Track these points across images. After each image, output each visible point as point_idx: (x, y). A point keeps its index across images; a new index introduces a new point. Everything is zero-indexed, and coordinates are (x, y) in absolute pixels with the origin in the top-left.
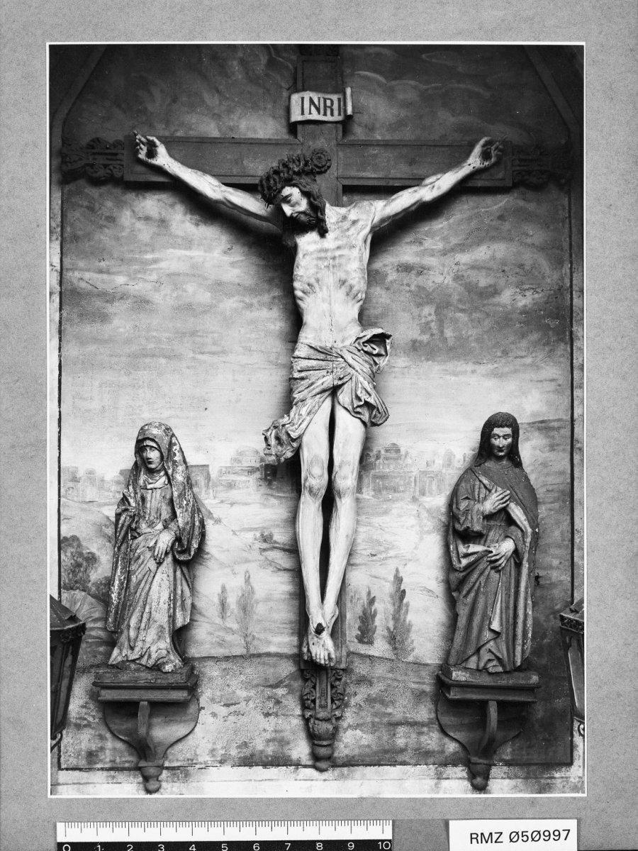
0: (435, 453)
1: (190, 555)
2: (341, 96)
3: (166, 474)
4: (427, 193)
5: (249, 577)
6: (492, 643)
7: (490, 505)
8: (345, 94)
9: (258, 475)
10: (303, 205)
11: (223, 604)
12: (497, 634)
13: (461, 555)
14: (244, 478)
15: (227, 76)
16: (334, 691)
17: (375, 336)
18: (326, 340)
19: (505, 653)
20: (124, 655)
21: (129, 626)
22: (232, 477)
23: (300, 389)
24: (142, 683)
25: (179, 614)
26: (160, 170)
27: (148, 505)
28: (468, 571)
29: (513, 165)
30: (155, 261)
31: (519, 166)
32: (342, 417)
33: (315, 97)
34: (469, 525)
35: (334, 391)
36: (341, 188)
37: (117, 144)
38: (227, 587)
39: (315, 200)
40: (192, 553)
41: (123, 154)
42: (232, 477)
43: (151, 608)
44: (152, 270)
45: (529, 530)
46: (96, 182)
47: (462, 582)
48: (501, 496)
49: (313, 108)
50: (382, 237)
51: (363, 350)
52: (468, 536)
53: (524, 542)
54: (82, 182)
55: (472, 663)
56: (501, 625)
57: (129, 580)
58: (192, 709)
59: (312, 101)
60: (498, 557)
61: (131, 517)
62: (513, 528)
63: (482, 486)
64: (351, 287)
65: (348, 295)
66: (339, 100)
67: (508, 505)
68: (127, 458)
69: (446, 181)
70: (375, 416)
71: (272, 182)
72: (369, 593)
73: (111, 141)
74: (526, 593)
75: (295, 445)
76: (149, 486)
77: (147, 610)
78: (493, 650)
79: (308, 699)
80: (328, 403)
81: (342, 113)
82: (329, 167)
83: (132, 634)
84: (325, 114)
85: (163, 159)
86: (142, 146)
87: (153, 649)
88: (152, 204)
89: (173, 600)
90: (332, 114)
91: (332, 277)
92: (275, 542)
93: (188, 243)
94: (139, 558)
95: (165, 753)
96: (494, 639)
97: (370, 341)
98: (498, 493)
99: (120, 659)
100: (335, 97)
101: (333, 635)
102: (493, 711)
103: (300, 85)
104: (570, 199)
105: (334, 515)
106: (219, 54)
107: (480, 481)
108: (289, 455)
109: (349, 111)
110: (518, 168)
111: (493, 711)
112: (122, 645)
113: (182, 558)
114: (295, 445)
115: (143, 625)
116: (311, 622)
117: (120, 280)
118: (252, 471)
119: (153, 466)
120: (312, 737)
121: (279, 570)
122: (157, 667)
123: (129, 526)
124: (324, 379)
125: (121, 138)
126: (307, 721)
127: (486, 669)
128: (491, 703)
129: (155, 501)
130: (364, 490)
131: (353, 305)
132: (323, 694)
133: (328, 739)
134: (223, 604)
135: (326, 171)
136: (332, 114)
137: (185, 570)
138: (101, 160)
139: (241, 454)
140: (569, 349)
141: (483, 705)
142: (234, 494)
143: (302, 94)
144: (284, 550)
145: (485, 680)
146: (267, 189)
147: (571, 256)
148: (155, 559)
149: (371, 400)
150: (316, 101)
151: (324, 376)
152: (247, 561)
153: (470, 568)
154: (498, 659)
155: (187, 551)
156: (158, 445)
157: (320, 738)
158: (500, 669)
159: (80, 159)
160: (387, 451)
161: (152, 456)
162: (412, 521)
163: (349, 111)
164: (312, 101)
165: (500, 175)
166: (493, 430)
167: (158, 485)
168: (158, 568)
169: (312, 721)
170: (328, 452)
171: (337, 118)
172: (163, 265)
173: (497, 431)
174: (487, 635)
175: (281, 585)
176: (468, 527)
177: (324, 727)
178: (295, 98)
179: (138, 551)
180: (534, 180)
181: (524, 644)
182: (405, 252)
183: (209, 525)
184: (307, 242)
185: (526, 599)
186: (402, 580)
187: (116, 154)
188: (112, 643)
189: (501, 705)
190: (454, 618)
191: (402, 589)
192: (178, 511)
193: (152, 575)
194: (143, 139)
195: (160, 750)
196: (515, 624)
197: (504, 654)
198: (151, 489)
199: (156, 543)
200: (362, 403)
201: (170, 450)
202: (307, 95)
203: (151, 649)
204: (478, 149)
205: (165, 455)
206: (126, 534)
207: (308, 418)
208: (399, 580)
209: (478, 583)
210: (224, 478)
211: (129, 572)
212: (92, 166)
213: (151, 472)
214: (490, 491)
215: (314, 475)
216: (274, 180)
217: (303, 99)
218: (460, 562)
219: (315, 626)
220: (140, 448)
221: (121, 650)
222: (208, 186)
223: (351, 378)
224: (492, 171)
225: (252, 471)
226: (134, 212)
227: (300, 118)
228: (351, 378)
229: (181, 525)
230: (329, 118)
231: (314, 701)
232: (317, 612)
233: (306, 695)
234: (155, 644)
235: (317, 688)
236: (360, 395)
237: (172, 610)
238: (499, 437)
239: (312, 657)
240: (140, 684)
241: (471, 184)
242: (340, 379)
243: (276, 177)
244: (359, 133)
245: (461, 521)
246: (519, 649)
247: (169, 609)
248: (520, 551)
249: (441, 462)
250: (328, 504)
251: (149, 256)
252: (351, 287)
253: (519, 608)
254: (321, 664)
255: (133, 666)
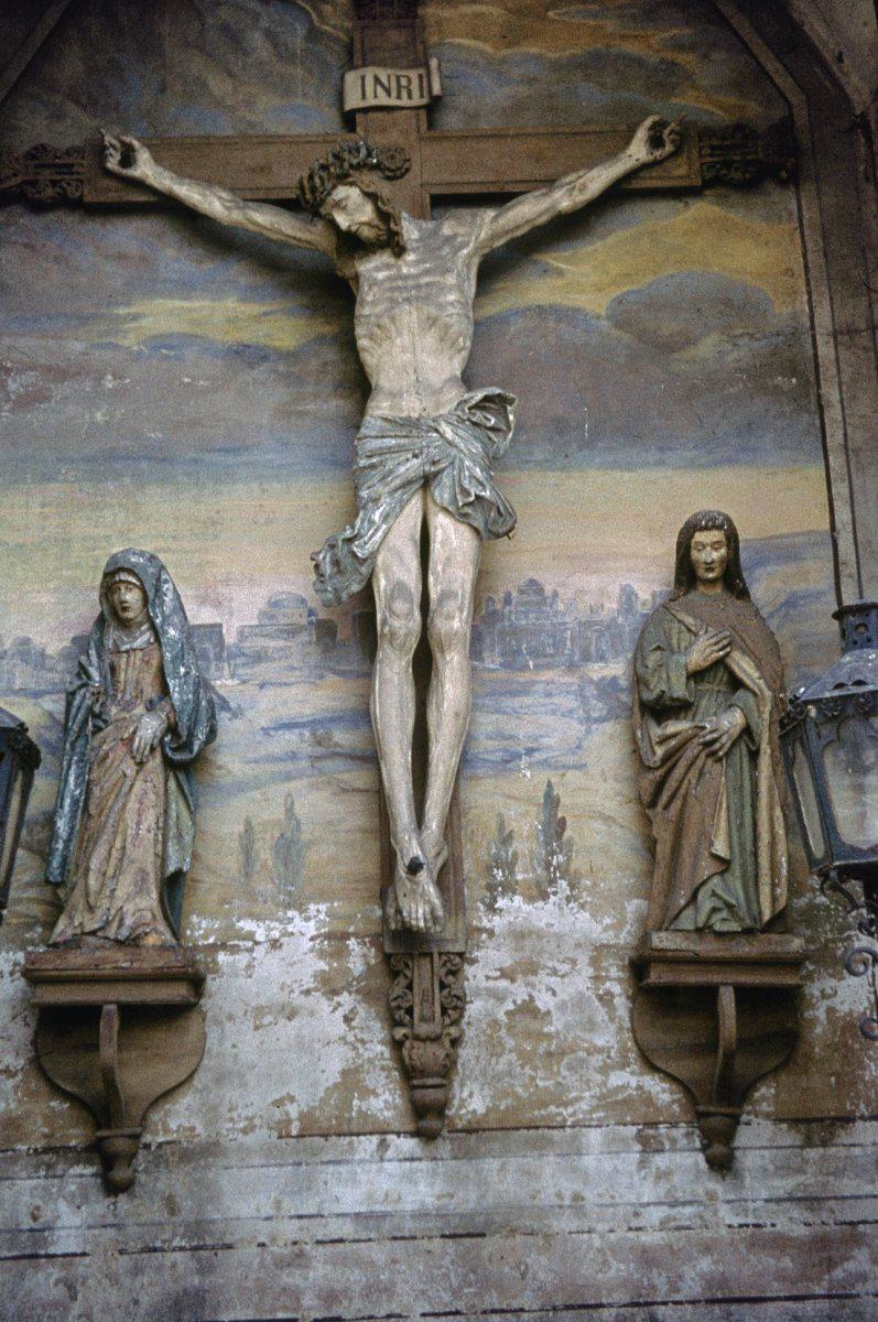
0: (602, 593)
1: (191, 751)
2: (422, 71)
3: (153, 627)
4: (564, 200)
5: (292, 803)
6: (716, 880)
7: (700, 653)
8: (427, 66)
9: (304, 637)
10: (367, 213)
11: (247, 851)
12: (725, 864)
13: (655, 739)
14: (281, 643)
15: (246, 53)
16: (445, 992)
17: (486, 399)
18: (411, 407)
19: (741, 894)
20: (77, 924)
21: (88, 869)
22: (261, 642)
23: (370, 483)
24: (107, 969)
25: (172, 849)
26: (140, 185)
27: (122, 677)
28: (669, 764)
29: (701, 156)
30: (136, 317)
31: (711, 155)
32: (443, 525)
33: (383, 75)
34: (664, 688)
35: (427, 482)
36: (428, 200)
37: (79, 151)
38: (254, 822)
39: (383, 203)
40: (196, 748)
41: (82, 165)
42: (261, 642)
43: (125, 840)
44: (126, 332)
45: (768, 694)
46: (38, 207)
47: (659, 787)
48: (713, 641)
49: (379, 89)
50: (494, 268)
51: (469, 420)
52: (661, 710)
53: (760, 713)
54: (16, 209)
55: (687, 921)
56: (731, 847)
57: (88, 792)
58: (193, 1025)
59: (377, 80)
60: (715, 735)
61: (93, 694)
62: (740, 693)
63: (683, 628)
64: (447, 327)
65: (442, 340)
66: (420, 77)
67: (727, 654)
68: (88, 605)
69: (597, 180)
70: (494, 522)
71: (317, 181)
72: (501, 826)
73: (64, 149)
74: (771, 797)
75: (364, 570)
76: (124, 648)
77: (118, 844)
78: (719, 892)
79: (399, 1008)
80: (415, 506)
81: (425, 93)
82: (407, 170)
83: (93, 882)
84: (399, 97)
85: (146, 168)
86: (113, 152)
87: (129, 908)
88: (127, 235)
89: (163, 827)
90: (410, 97)
91: (415, 314)
92: (337, 745)
93: (185, 288)
94: (106, 756)
95: (144, 1118)
96: (722, 873)
97: (477, 406)
98: (710, 634)
99: (70, 932)
100: (414, 74)
101: (440, 882)
102: (727, 1000)
103: (357, 60)
104: (799, 201)
105: (434, 682)
106: (7, 1214)
107: (680, 621)
108: (356, 588)
109: (437, 89)
110: (710, 159)
111: (727, 1000)
112: (74, 908)
113: (177, 757)
114: (364, 570)
115: (110, 872)
116: (399, 856)
117: (76, 346)
118: (292, 631)
119: (130, 615)
120: (410, 1074)
121: (345, 791)
122: (132, 942)
123: (90, 710)
124: (409, 465)
125: (78, 142)
126: (397, 1045)
127: (711, 927)
128: (722, 990)
129: (136, 673)
130: (486, 654)
131: (451, 358)
132: (427, 998)
133: (438, 1075)
134: (247, 851)
135: (403, 176)
136: (410, 97)
137: (182, 777)
138: (46, 174)
139: (275, 604)
140: (818, 422)
141: (709, 994)
142: (263, 670)
143: (360, 72)
144: (352, 757)
145: (709, 948)
146: (307, 203)
147: (808, 283)
148: (134, 758)
149: (487, 494)
150: (384, 80)
151: (408, 460)
152: (289, 777)
153: (671, 758)
154: (730, 906)
155: (187, 746)
156: (139, 579)
157: (423, 1073)
158: (735, 927)
159: (15, 175)
160: (521, 592)
161: (124, 600)
162: (569, 702)
163: (437, 89)
164: (377, 80)
165: (682, 171)
166: (692, 536)
167: (138, 643)
168: (138, 772)
169: (407, 1044)
170: (420, 576)
171: (417, 101)
172: (144, 322)
173: (699, 537)
174: (707, 867)
175: (353, 816)
176: (663, 692)
177: (432, 1095)
178: (351, 78)
179: (105, 747)
180: (737, 175)
181: (774, 886)
182: (535, 289)
183: (223, 716)
184: (374, 270)
185: (771, 808)
186: (558, 802)
187: (72, 165)
188: (57, 907)
189: (742, 993)
190: (651, 845)
191: (560, 815)
192: (171, 683)
193: (128, 783)
194: (114, 142)
195: (136, 1111)
196: (755, 854)
197: (737, 894)
198: (127, 652)
199: (134, 733)
200: (472, 499)
201: (158, 589)
202: (370, 73)
203: (125, 909)
204: (641, 134)
205: (151, 595)
206: (85, 722)
207: (384, 527)
208: (551, 801)
209: (686, 782)
210: (248, 644)
211: (89, 783)
212: (34, 183)
213: (125, 624)
214: (696, 635)
215: (398, 621)
216: (321, 178)
217: (363, 78)
218: (654, 753)
219: (407, 862)
220: (109, 587)
221: (71, 918)
222: (214, 203)
223: (452, 463)
224: (668, 164)
225: (292, 631)
226: (98, 248)
227: (362, 104)
228: (452, 463)
229: (177, 703)
230: (405, 102)
231: (410, 1011)
232: (410, 839)
233: (395, 999)
234: (137, 905)
235: (416, 986)
236: (467, 486)
237: (160, 847)
238: (704, 546)
239: (403, 922)
240: (106, 972)
241: (636, 184)
242: (434, 463)
243: (324, 174)
244: (451, 121)
245: (652, 686)
246: (765, 890)
247: (156, 841)
248: (754, 728)
249: (615, 606)
250: (424, 666)
251: (122, 311)
252: (447, 327)
253: (760, 823)
254: (419, 929)
255: (90, 939)
